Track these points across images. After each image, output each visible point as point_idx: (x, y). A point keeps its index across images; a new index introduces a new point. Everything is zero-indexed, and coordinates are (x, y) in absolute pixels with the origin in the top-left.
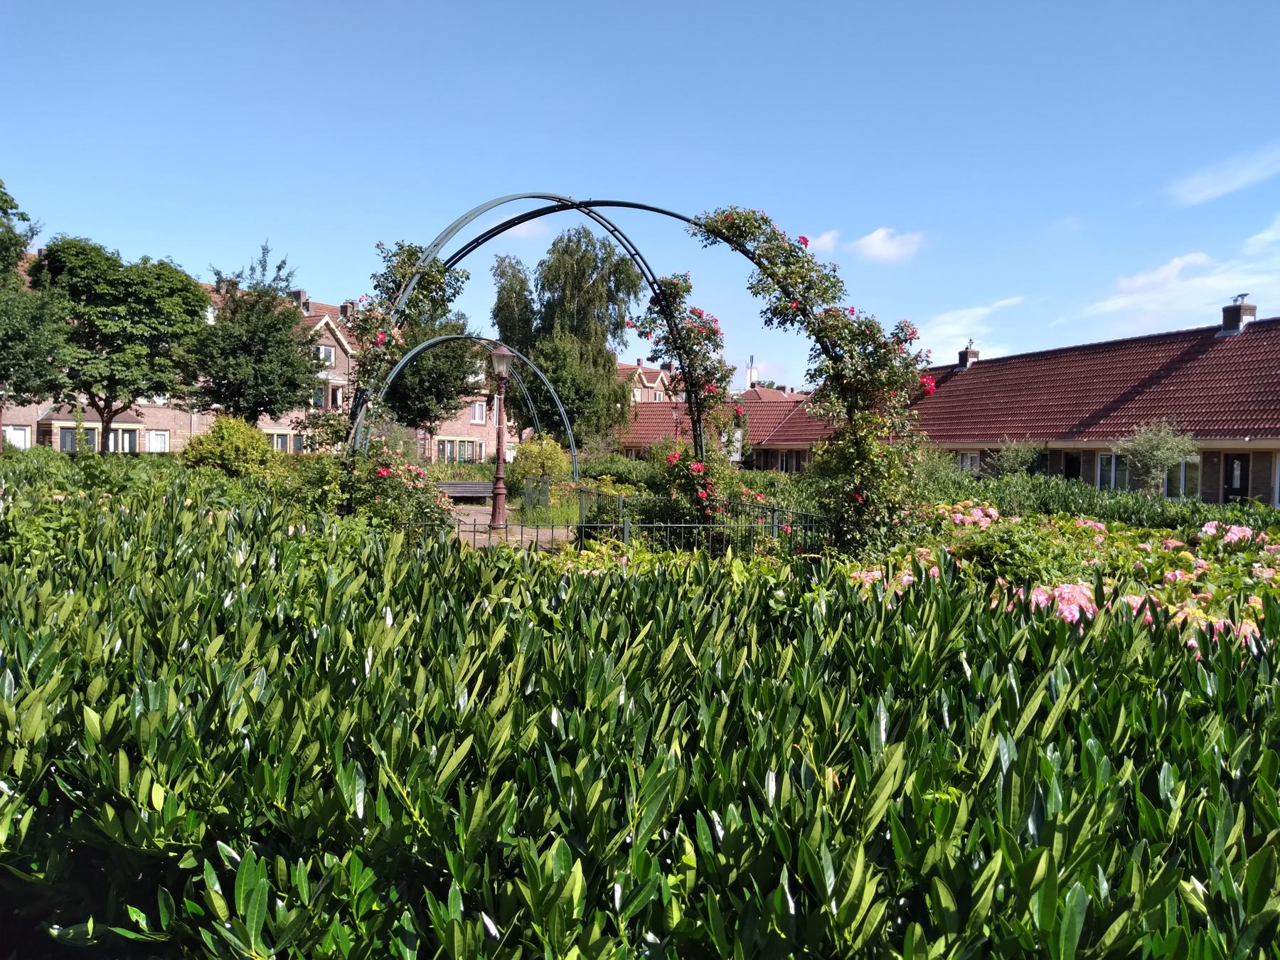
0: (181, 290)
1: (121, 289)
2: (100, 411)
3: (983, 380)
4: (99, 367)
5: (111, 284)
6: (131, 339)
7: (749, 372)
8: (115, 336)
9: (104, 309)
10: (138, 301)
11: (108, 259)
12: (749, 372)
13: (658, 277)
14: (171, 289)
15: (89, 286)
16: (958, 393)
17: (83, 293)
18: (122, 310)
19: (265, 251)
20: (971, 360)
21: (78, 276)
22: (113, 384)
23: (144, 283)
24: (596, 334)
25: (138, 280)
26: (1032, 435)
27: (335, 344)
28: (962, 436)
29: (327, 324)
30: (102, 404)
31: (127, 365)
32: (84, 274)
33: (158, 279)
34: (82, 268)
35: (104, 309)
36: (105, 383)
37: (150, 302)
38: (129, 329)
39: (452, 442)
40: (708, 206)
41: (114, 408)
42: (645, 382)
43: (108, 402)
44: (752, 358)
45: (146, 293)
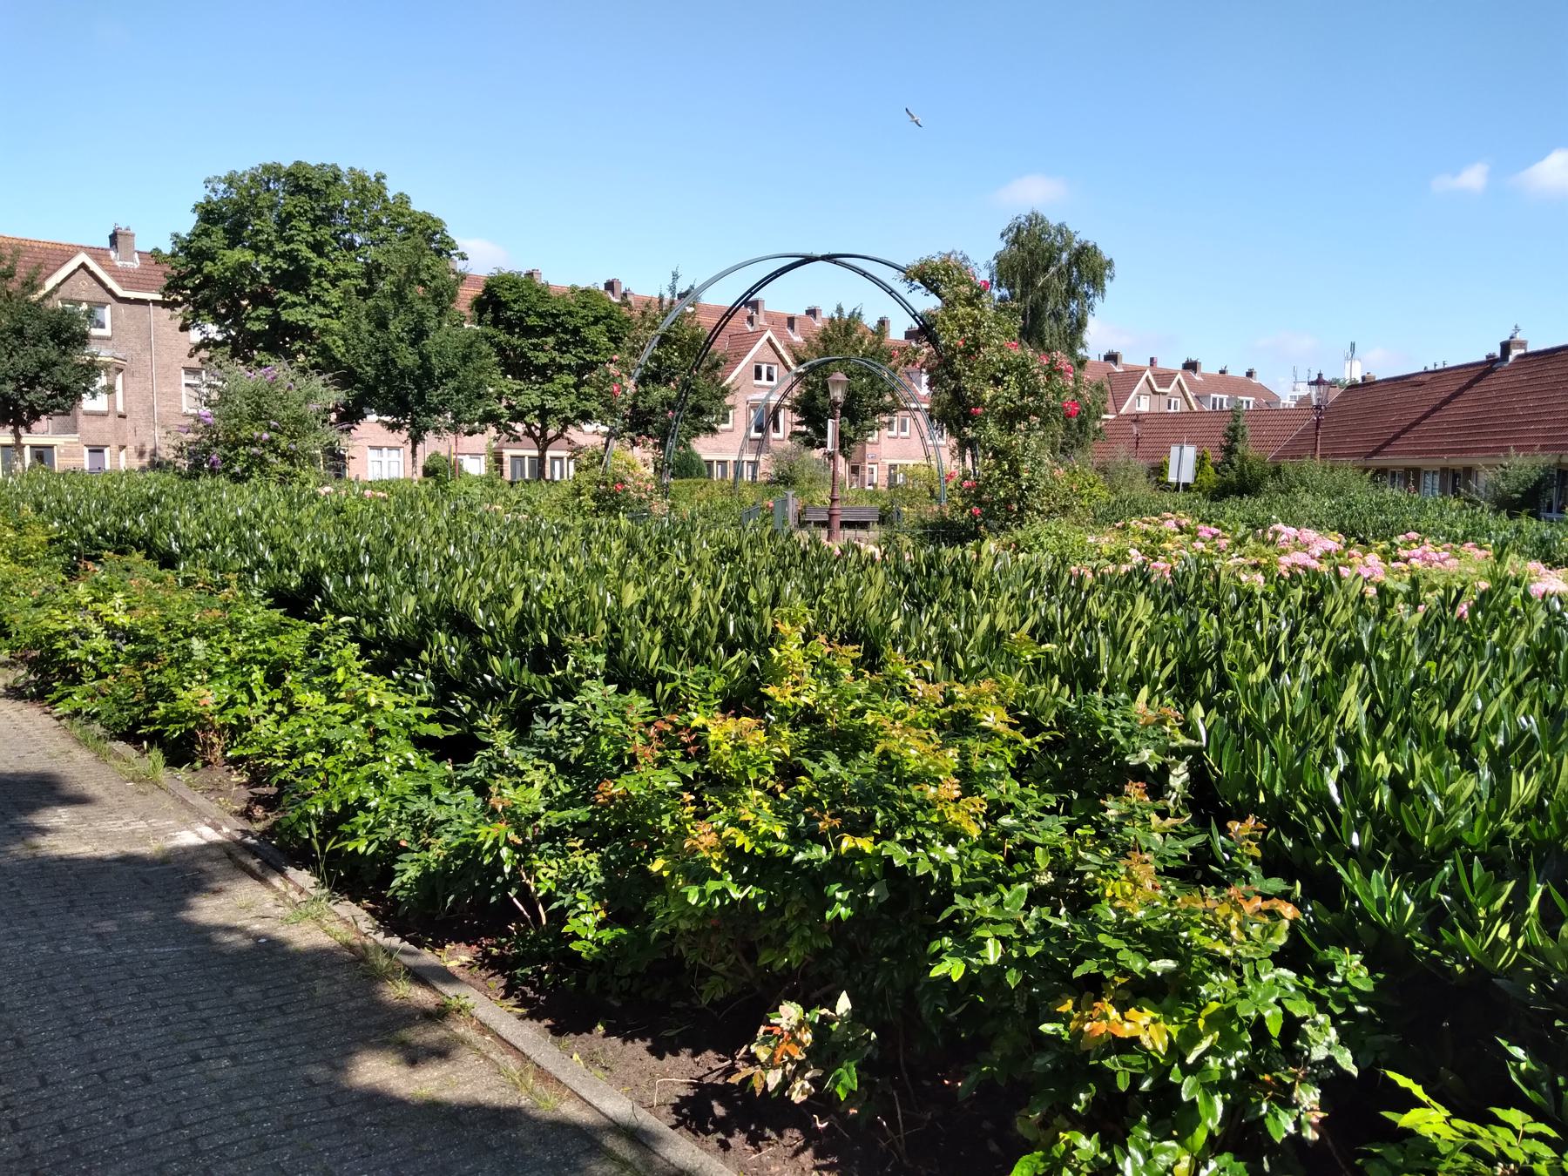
0: (605, 318)
1: (549, 320)
2: (536, 440)
3: (1521, 377)
4: (532, 398)
5: (540, 315)
6: (561, 368)
7: (1348, 366)
8: (545, 366)
9: (534, 341)
10: (565, 331)
11: (538, 291)
12: (1348, 366)
13: (919, 311)
14: (595, 317)
15: (521, 319)
16: (1489, 395)
17: (516, 325)
18: (551, 340)
19: (675, 276)
20: (1515, 352)
21: (511, 310)
22: (544, 413)
23: (570, 313)
24: (1051, 335)
25: (564, 311)
26: (1543, 448)
27: (778, 361)
28: (1476, 450)
29: (769, 340)
30: (538, 433)
31: (556, 395)
32: (516, 307)
33: (584, 308)
34: (515, 301)
35: (534, 341)
36: (537, 412)
37: (576, 331)
38: (558, 359)
39: (723, 463)
40: (910, 259)
41: (549, 437)
42: (1155, 386)
43: (544, 433)
44: (1353, 346)
45: (571, 323)
